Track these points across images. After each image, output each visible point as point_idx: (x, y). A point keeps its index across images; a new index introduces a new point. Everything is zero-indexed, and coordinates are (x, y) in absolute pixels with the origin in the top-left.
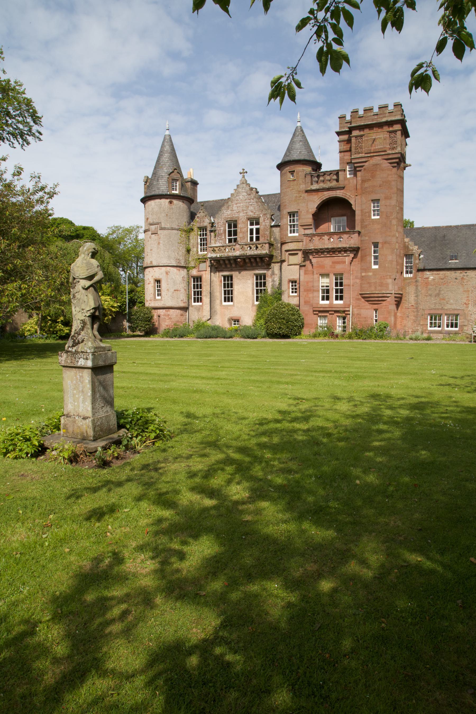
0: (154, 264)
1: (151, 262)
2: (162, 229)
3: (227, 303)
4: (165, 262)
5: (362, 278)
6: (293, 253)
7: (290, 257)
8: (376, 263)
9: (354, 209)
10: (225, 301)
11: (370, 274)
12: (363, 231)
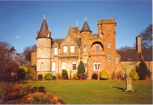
0: (41, 58)
1: (40, 57)
2: (44, 47)
3: (74, 70)
4: (45, 57)
5: (106, 64)
6: (86, 56)
7: (85, 57)
8: (110, 60)
9: (103, 45)
10: (73, 69)
11: (108, 62)
12: (105, 51)
